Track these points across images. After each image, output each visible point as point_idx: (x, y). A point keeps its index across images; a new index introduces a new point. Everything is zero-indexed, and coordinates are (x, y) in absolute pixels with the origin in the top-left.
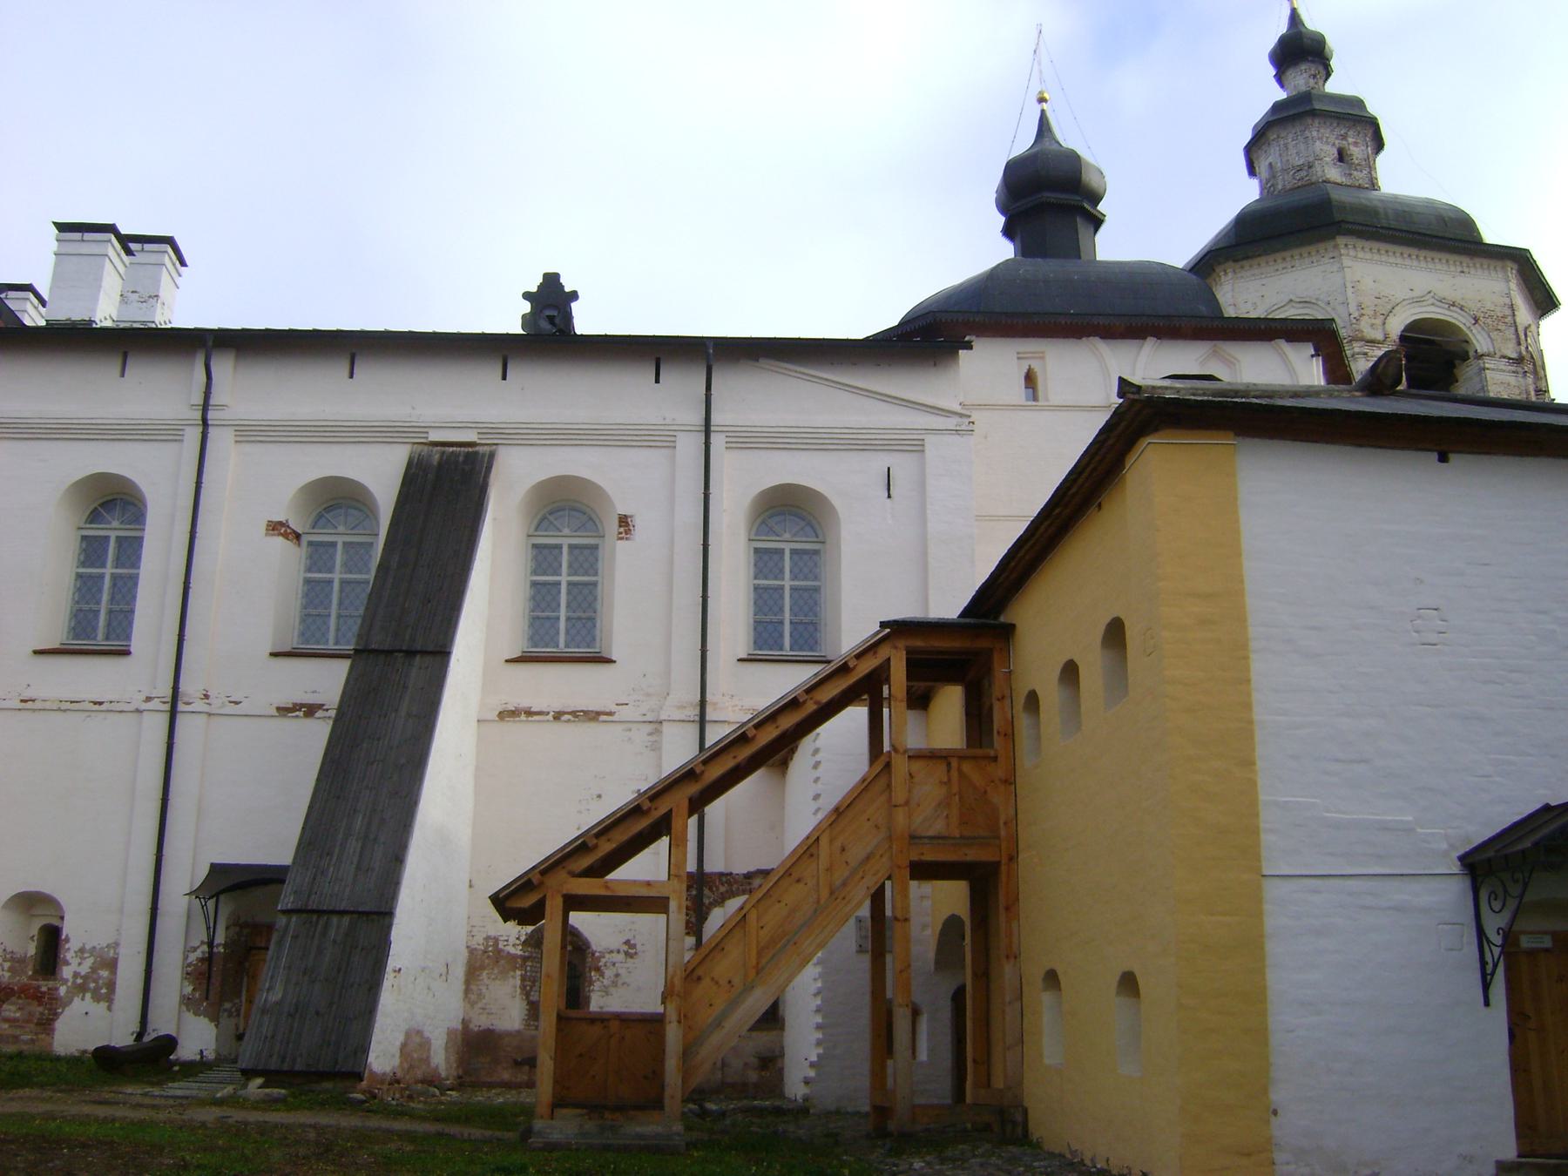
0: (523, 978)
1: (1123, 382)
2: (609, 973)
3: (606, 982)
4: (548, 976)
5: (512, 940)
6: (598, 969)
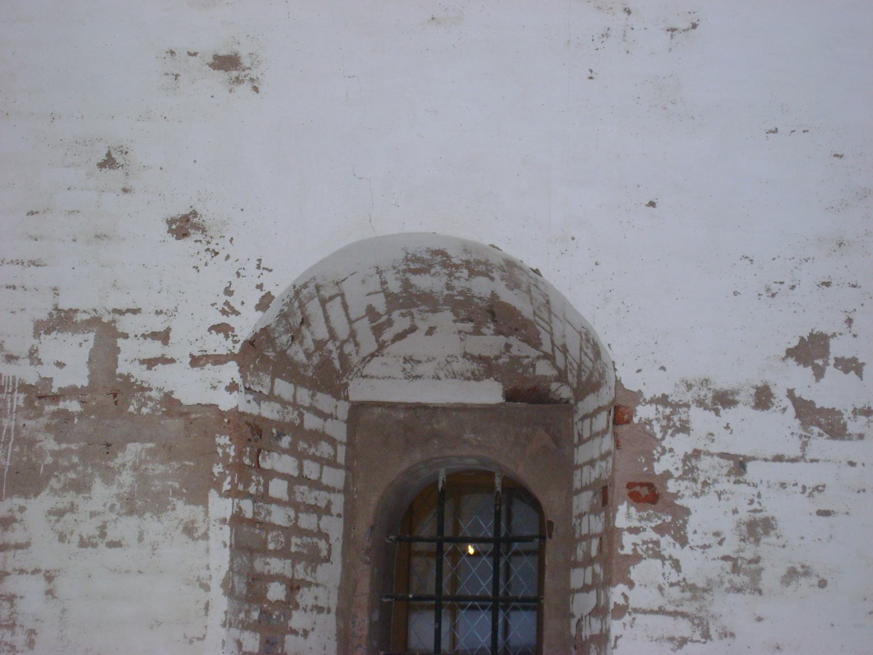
0: (248, 536)
1: (817, 380)
2: (710, 514)
3: (695, 565)
4: (849, 418)
5: (192, 333)
6: (648, 494)
